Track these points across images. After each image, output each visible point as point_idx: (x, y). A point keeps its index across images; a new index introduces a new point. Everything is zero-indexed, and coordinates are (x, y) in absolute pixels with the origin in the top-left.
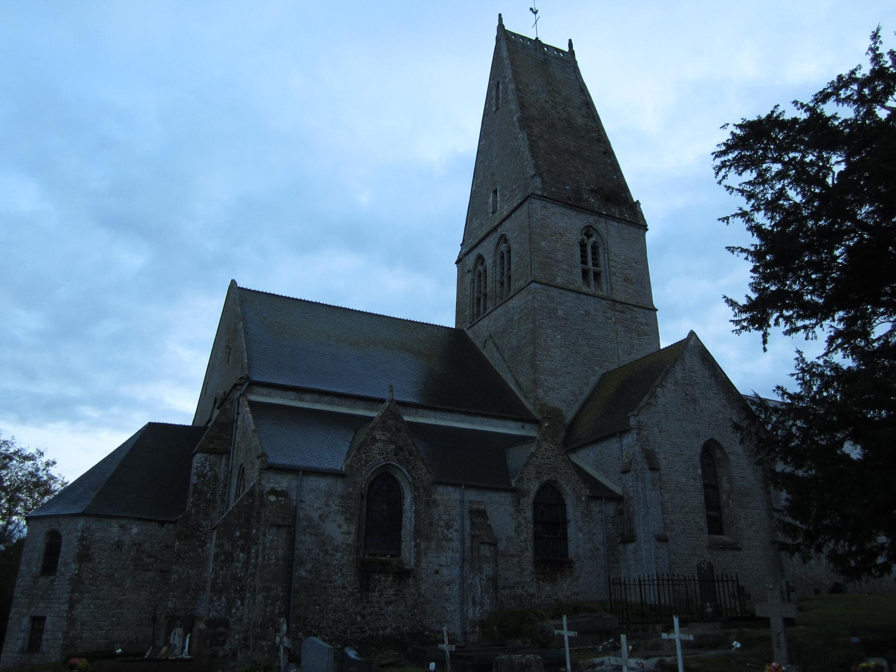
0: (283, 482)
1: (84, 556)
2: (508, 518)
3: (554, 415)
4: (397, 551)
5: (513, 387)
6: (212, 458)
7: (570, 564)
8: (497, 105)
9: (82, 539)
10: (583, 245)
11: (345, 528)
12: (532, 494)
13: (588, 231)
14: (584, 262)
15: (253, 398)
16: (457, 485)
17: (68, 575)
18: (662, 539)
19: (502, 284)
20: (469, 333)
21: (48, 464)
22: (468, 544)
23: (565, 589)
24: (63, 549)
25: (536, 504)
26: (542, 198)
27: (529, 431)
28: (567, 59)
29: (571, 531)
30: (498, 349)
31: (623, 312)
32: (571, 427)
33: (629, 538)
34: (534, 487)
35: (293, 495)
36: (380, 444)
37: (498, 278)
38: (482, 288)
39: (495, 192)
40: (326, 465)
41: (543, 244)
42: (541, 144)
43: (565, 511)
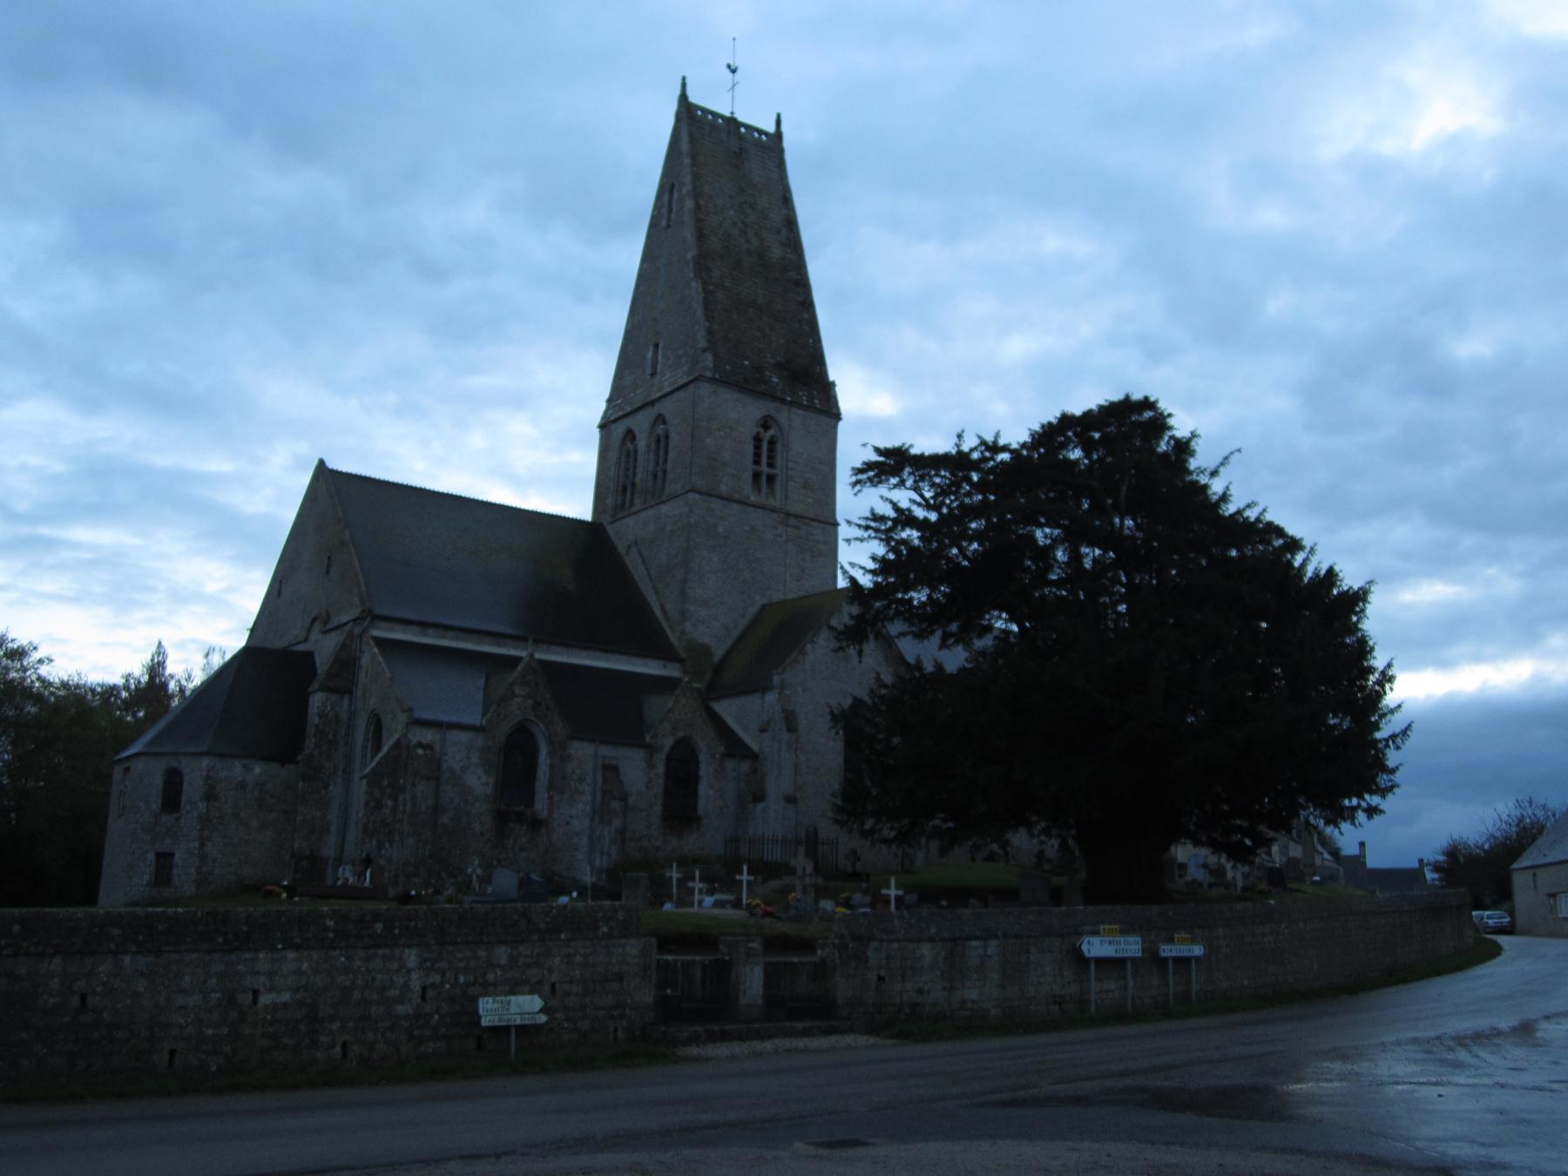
0: (428, 736)
1: (210, 796)
2: (640, 773)
3: (699, 652)
4: (530, 800)
5: (658, 613)
6: (334, 697)
7: (698, 819)
8: (669, 220)
9: (207, 778)
10: (757, 440)
11: (484, 779)
12: (666, 750)
13: (766, 424)
14: (757, 462)
15: (377, 633)
16: (591, 741)
17: (196, 814)
18: (791, 800)
19: (655, 476)
20: (610, 530)
21: (40, 661)
22: (599, 795)
23: (691, 843)
24: (185, 786)
25: (669, 759)
26: (712, 380)
27: (671, 671)
28: (772, 145)
29: (703, 788)
30: (644, 561)
31: (797, 527)
32: (719, 669)
33: (759, 797)
34: (668, 743)
35: (437, 747)
36: (519, 700)
37: (651, 468)
38: (630, 474)
39: (656, 346)
40: (467, 720)
41: (708, 441)
42: (720, 295)
43: (697, 768)
